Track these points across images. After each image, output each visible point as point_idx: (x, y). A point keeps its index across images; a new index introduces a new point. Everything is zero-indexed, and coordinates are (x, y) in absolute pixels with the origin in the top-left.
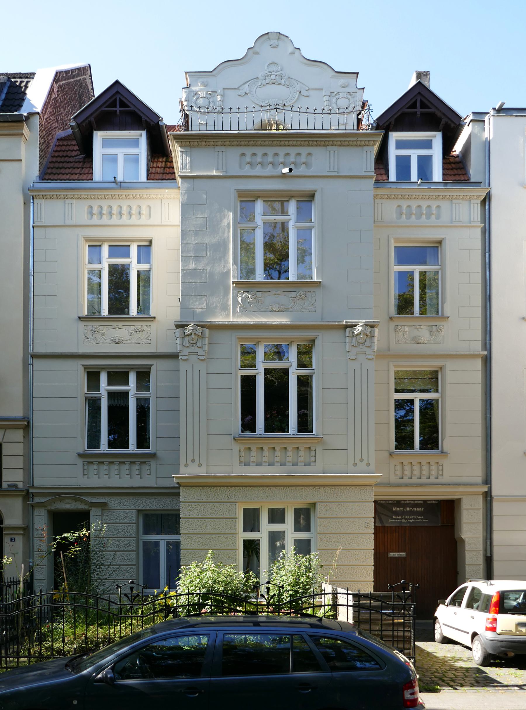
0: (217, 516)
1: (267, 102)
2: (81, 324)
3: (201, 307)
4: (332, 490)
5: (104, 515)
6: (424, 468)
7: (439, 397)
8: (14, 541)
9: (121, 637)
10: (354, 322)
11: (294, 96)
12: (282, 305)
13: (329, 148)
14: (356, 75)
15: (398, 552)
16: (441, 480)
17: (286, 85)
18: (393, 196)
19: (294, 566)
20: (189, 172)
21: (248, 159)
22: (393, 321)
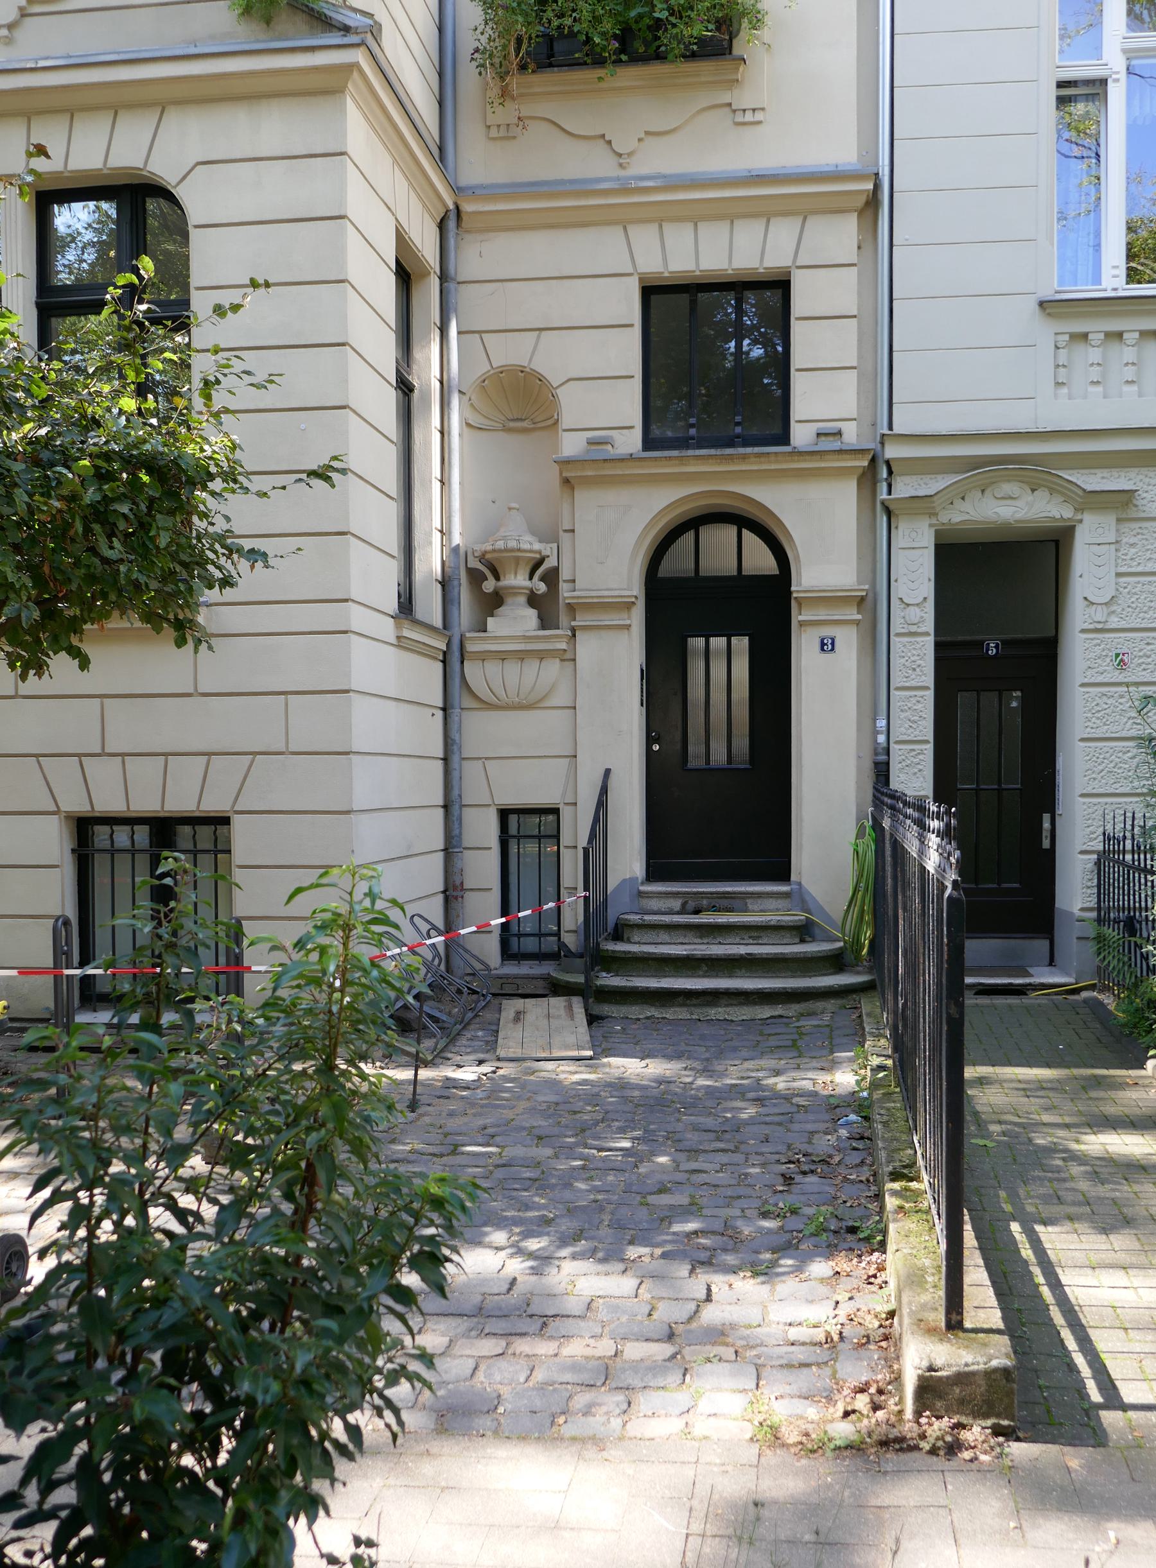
5: (1125, 540)
8: (833, 649)
9: (113, 1233)
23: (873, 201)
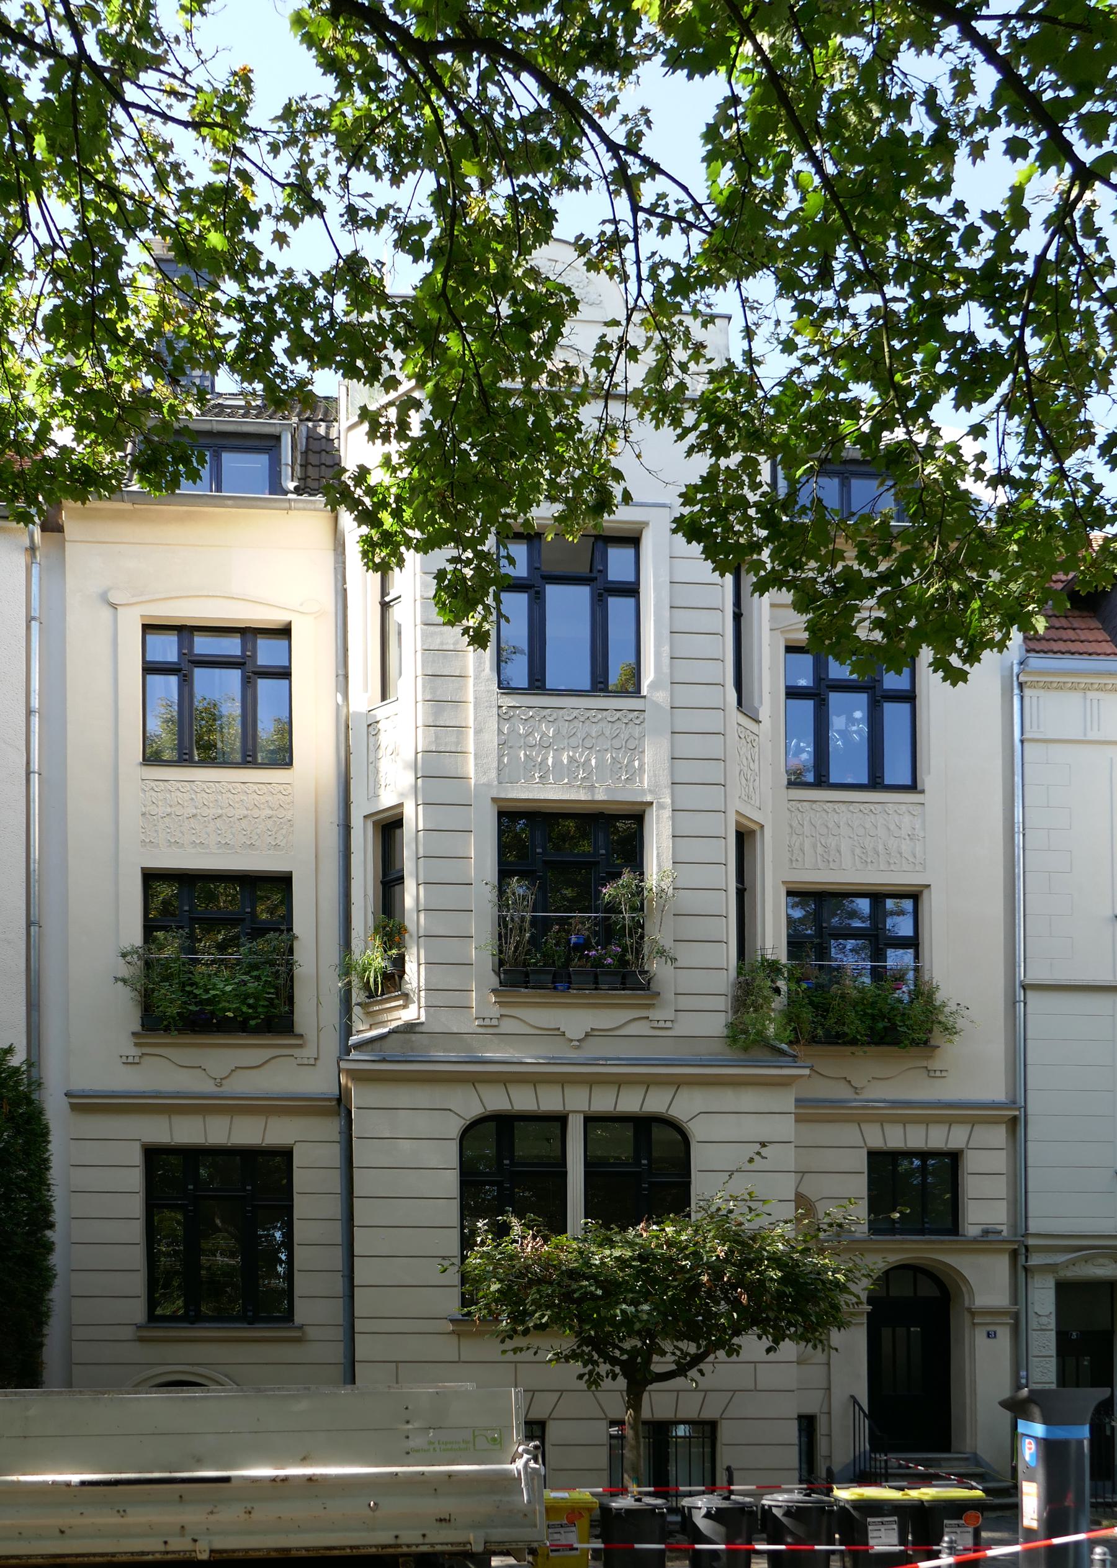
19: (720, 1219)
23: (1014, 1120)
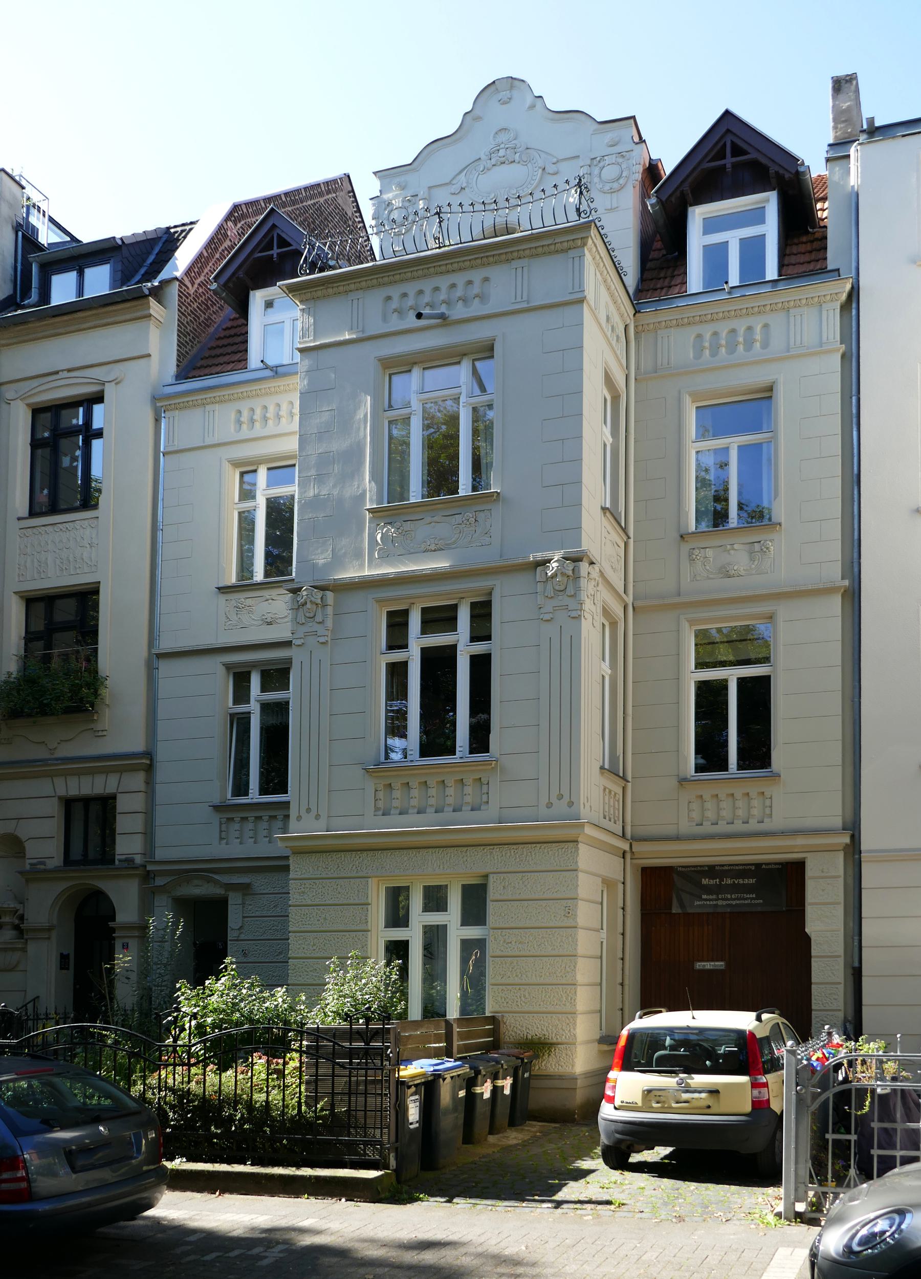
0: (340, 902)
1: (493, 195)
2: (223, 598)
3: (323, 557)
4: (512, 851)
6: (739, 804)
7: (771, 672)
10: (546, 555)
11: (534, 178)
12: (440, 539)
13: (516, 263)
14: (632, 121)
15: (712, 960)
16: (767, 826)
17: (522, 162)
18: (686, 320)
20: (311, 341)
21: (394, 304)
22: (687, 541)
